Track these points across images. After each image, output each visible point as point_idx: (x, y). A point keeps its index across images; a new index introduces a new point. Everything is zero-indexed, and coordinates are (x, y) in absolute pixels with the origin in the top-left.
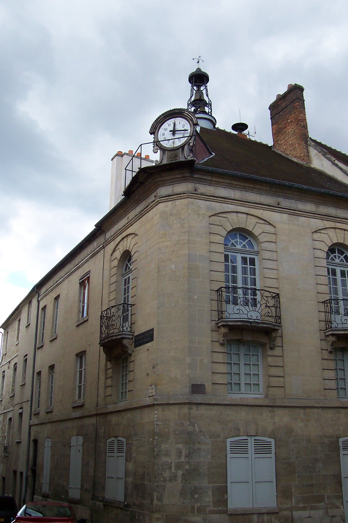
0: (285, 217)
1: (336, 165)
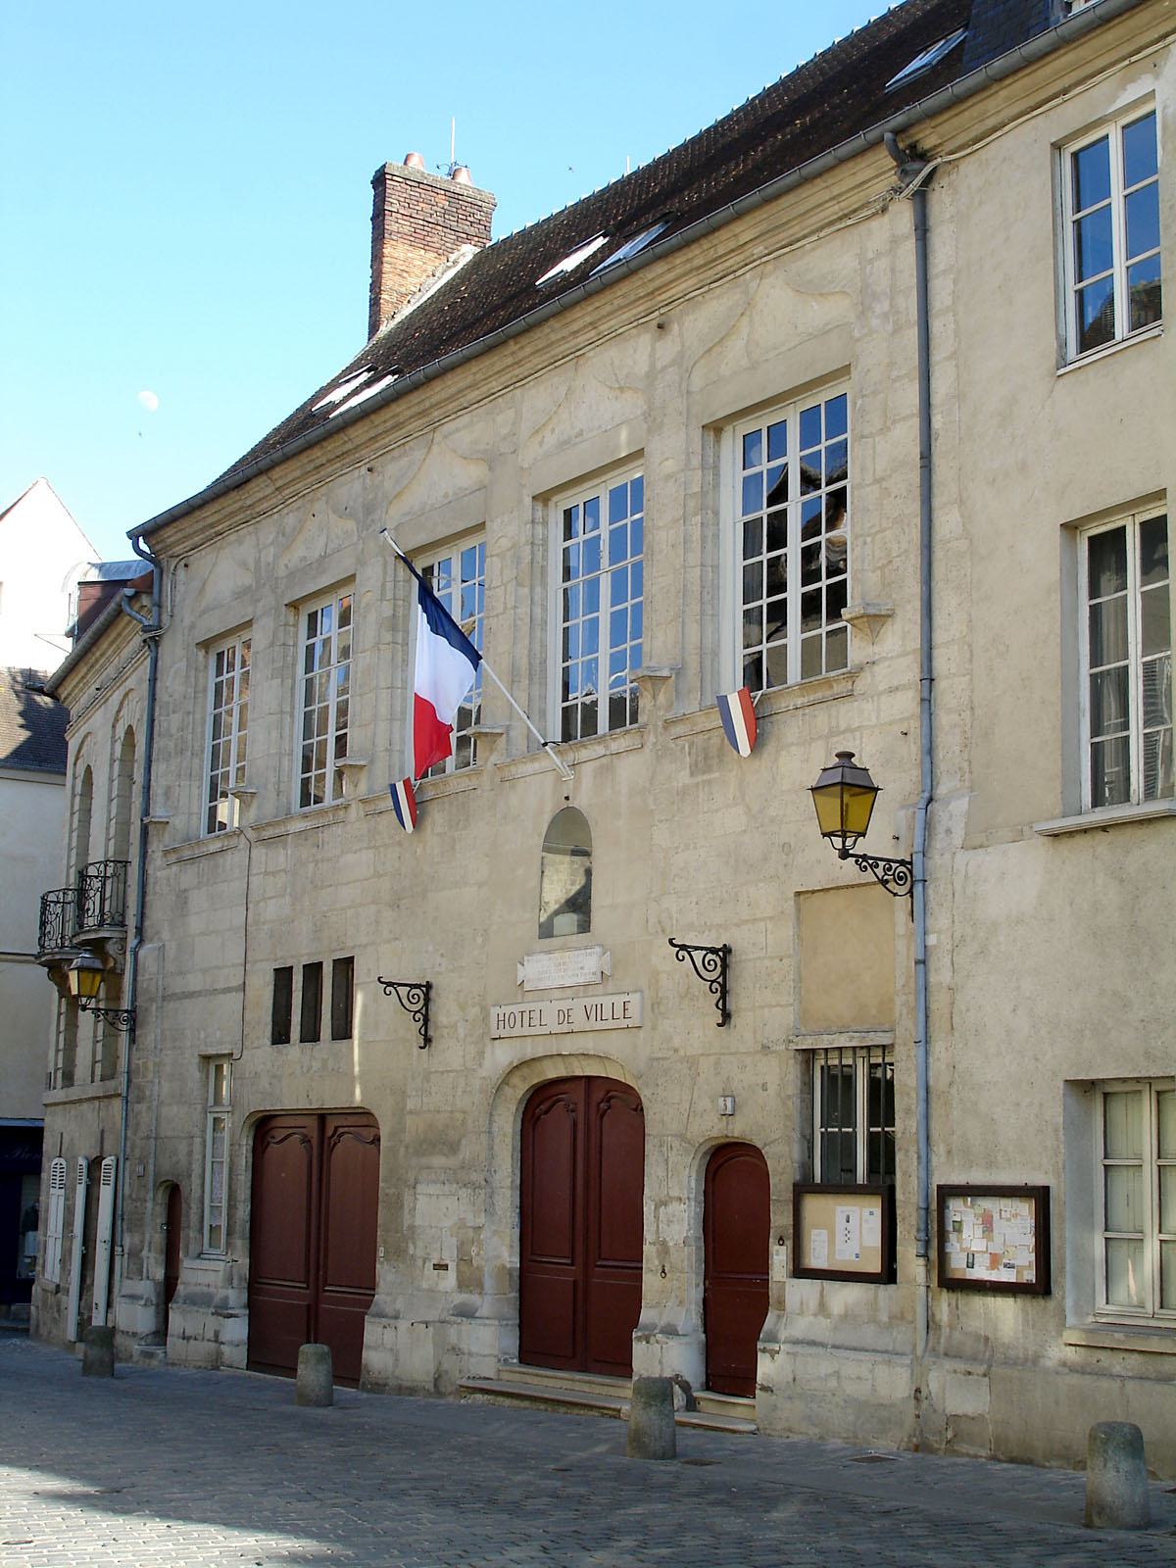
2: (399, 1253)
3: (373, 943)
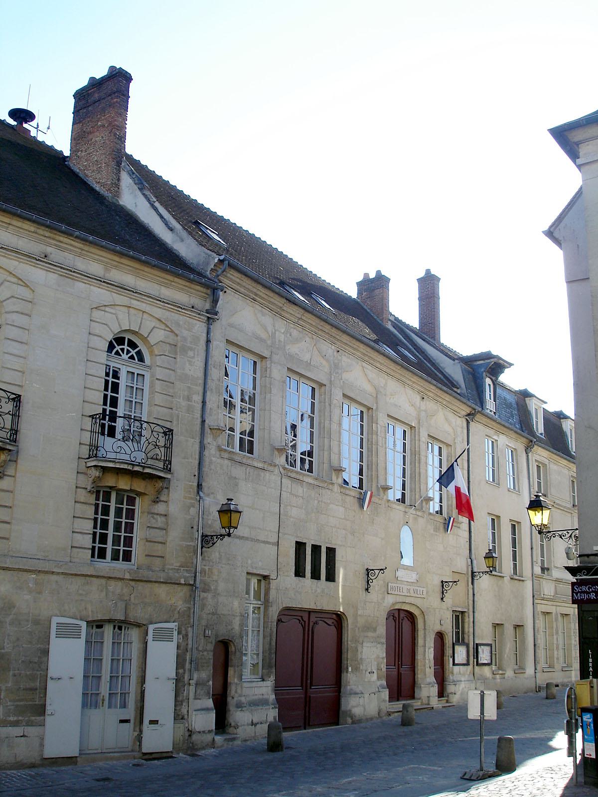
0: (52, 278)
1: (156, 209)
2: (356, 669)
3: (344, 546)
